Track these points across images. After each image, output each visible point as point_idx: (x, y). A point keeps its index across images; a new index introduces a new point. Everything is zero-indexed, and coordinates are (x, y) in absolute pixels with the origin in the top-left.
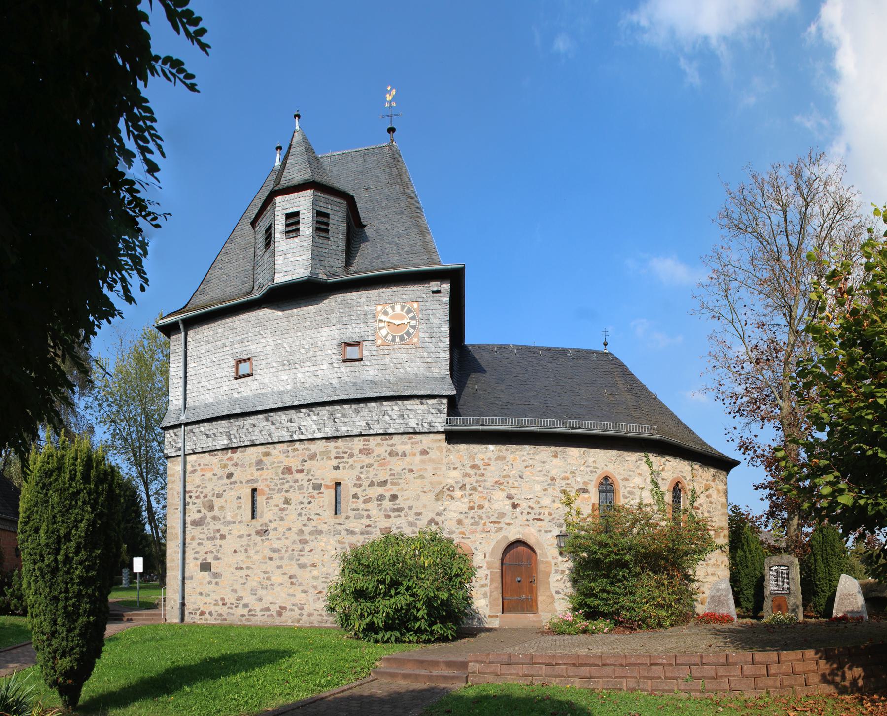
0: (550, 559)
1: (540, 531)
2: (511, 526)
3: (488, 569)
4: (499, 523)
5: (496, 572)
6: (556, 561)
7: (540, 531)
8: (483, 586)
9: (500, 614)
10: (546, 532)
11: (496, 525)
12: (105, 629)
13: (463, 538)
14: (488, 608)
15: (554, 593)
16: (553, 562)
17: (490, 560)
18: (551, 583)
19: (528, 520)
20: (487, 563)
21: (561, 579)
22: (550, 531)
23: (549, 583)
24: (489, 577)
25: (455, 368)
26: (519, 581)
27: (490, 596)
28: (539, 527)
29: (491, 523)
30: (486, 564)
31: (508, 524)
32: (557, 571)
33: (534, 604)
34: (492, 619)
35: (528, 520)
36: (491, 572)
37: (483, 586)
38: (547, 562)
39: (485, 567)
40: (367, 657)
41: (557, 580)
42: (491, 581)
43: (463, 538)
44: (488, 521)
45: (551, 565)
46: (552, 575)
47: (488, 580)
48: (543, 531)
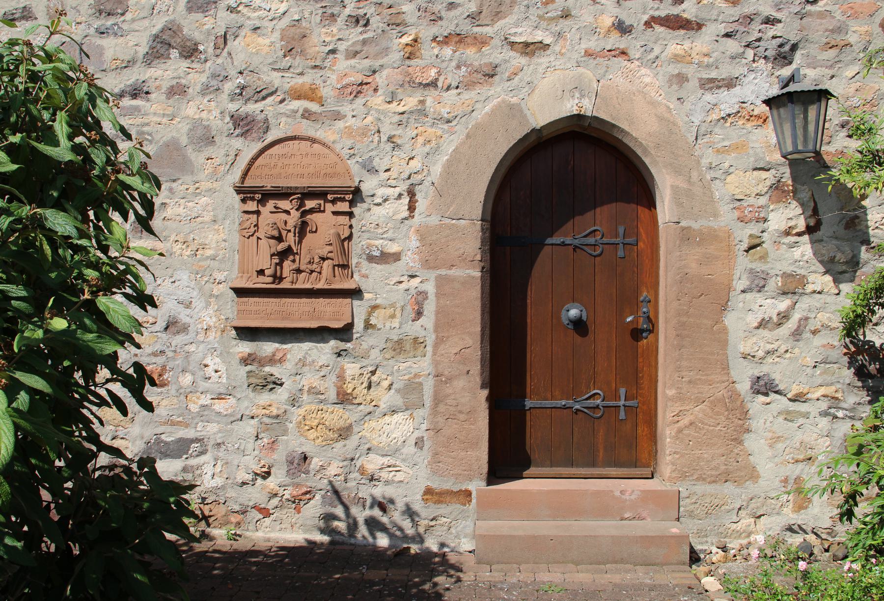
0: (726, 217)
1: (681, 79)
2: (542, 60)
3: (427, 264)
4: (481, 42)
5: (466, 282)
6: (753, 229)
7: (681, 79)
8: (399, 347)
9: (477, 486)
10: (710, 84)
11: (470, 53)
12: (78, 136)
13: (307, 115)
14: (424, 457)
15: (744, 387)
16: (744, 234)
17: (434, 220)
18: (732, 338)
19: (622, 28)
20: (423, 234)
21: (784, 317)
22: (730, 83)
23: (721, 339)
24: (430, 308)
25: (653, 395)
26: (579, 326)
27: (438, 400)
28: (677, 59)
29: (446, 40)
30: (414, 242)
31: (529, 48)
32: (758, 284)
33: (642, 430)
34: (443, 509)
35: (622, 28)
36: (441, 282)
37: (399, 347)
38: (709, 237)
39: (410, 260)
40: (223, 317)
41: (762, 324)
42: (443, 323)
43: (307, 115)
44: (427, 32)
45: (729, 248)
46: (738, 301)
47: (428, 320)
48: (694, 83)
